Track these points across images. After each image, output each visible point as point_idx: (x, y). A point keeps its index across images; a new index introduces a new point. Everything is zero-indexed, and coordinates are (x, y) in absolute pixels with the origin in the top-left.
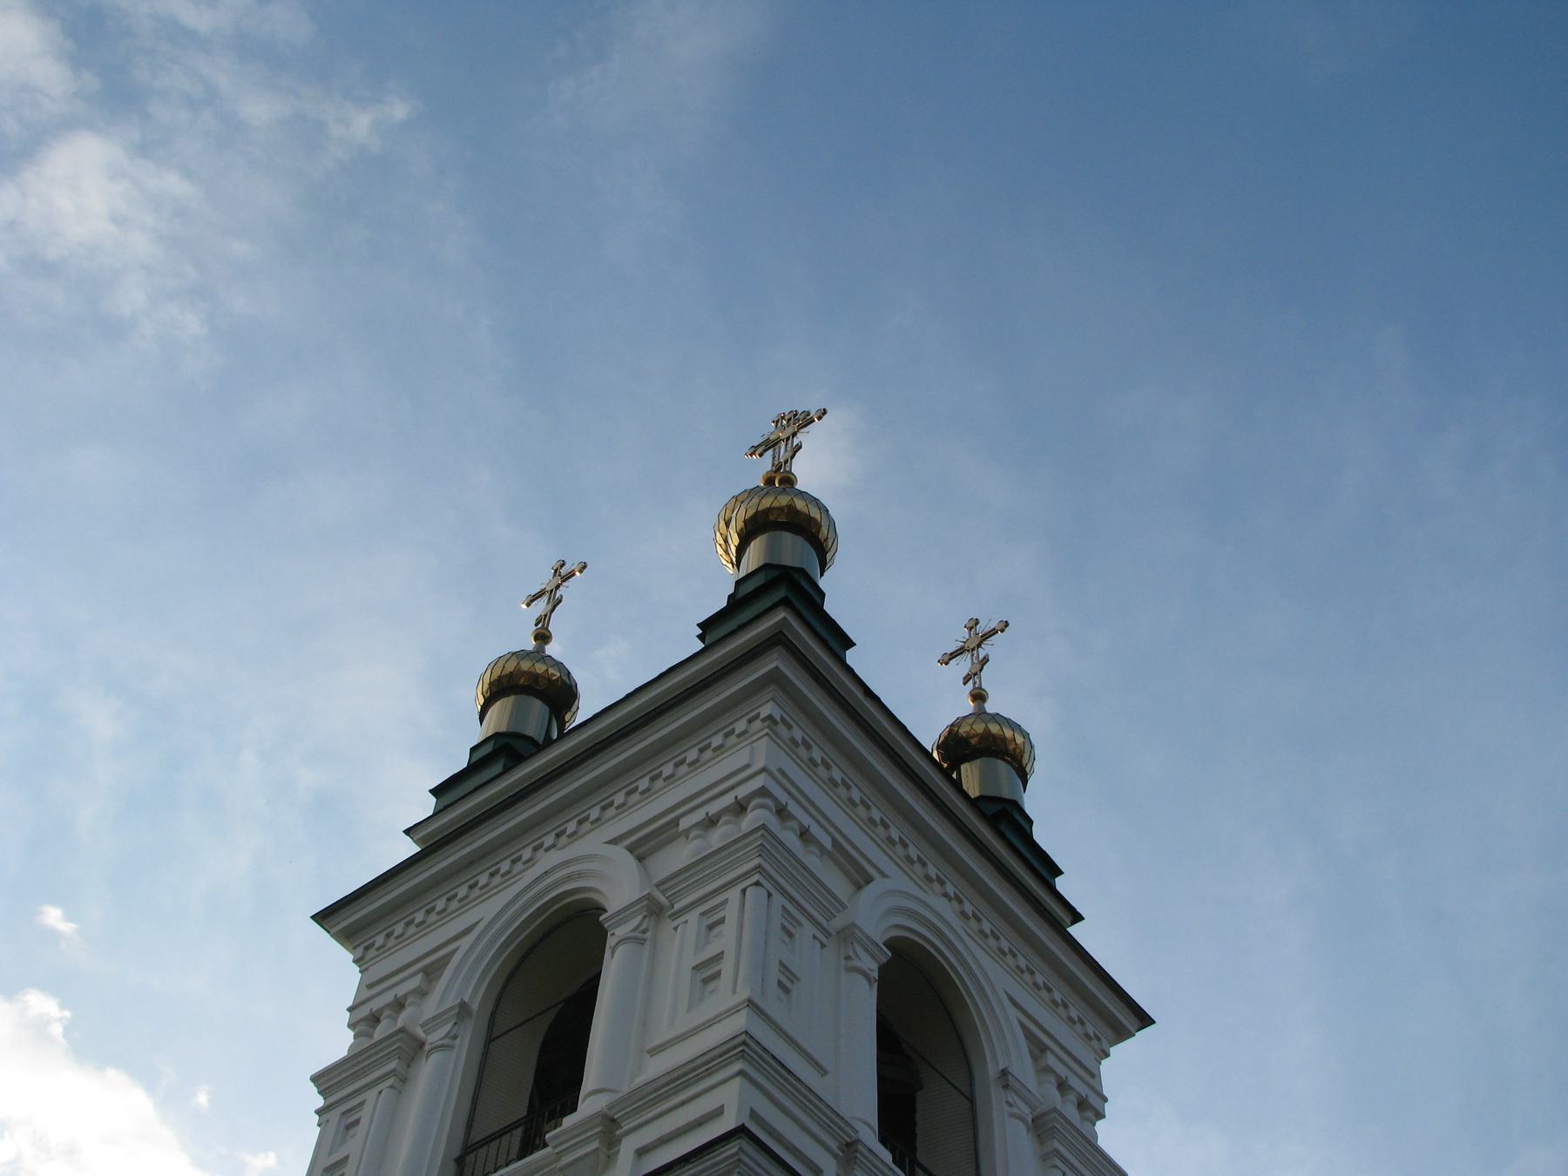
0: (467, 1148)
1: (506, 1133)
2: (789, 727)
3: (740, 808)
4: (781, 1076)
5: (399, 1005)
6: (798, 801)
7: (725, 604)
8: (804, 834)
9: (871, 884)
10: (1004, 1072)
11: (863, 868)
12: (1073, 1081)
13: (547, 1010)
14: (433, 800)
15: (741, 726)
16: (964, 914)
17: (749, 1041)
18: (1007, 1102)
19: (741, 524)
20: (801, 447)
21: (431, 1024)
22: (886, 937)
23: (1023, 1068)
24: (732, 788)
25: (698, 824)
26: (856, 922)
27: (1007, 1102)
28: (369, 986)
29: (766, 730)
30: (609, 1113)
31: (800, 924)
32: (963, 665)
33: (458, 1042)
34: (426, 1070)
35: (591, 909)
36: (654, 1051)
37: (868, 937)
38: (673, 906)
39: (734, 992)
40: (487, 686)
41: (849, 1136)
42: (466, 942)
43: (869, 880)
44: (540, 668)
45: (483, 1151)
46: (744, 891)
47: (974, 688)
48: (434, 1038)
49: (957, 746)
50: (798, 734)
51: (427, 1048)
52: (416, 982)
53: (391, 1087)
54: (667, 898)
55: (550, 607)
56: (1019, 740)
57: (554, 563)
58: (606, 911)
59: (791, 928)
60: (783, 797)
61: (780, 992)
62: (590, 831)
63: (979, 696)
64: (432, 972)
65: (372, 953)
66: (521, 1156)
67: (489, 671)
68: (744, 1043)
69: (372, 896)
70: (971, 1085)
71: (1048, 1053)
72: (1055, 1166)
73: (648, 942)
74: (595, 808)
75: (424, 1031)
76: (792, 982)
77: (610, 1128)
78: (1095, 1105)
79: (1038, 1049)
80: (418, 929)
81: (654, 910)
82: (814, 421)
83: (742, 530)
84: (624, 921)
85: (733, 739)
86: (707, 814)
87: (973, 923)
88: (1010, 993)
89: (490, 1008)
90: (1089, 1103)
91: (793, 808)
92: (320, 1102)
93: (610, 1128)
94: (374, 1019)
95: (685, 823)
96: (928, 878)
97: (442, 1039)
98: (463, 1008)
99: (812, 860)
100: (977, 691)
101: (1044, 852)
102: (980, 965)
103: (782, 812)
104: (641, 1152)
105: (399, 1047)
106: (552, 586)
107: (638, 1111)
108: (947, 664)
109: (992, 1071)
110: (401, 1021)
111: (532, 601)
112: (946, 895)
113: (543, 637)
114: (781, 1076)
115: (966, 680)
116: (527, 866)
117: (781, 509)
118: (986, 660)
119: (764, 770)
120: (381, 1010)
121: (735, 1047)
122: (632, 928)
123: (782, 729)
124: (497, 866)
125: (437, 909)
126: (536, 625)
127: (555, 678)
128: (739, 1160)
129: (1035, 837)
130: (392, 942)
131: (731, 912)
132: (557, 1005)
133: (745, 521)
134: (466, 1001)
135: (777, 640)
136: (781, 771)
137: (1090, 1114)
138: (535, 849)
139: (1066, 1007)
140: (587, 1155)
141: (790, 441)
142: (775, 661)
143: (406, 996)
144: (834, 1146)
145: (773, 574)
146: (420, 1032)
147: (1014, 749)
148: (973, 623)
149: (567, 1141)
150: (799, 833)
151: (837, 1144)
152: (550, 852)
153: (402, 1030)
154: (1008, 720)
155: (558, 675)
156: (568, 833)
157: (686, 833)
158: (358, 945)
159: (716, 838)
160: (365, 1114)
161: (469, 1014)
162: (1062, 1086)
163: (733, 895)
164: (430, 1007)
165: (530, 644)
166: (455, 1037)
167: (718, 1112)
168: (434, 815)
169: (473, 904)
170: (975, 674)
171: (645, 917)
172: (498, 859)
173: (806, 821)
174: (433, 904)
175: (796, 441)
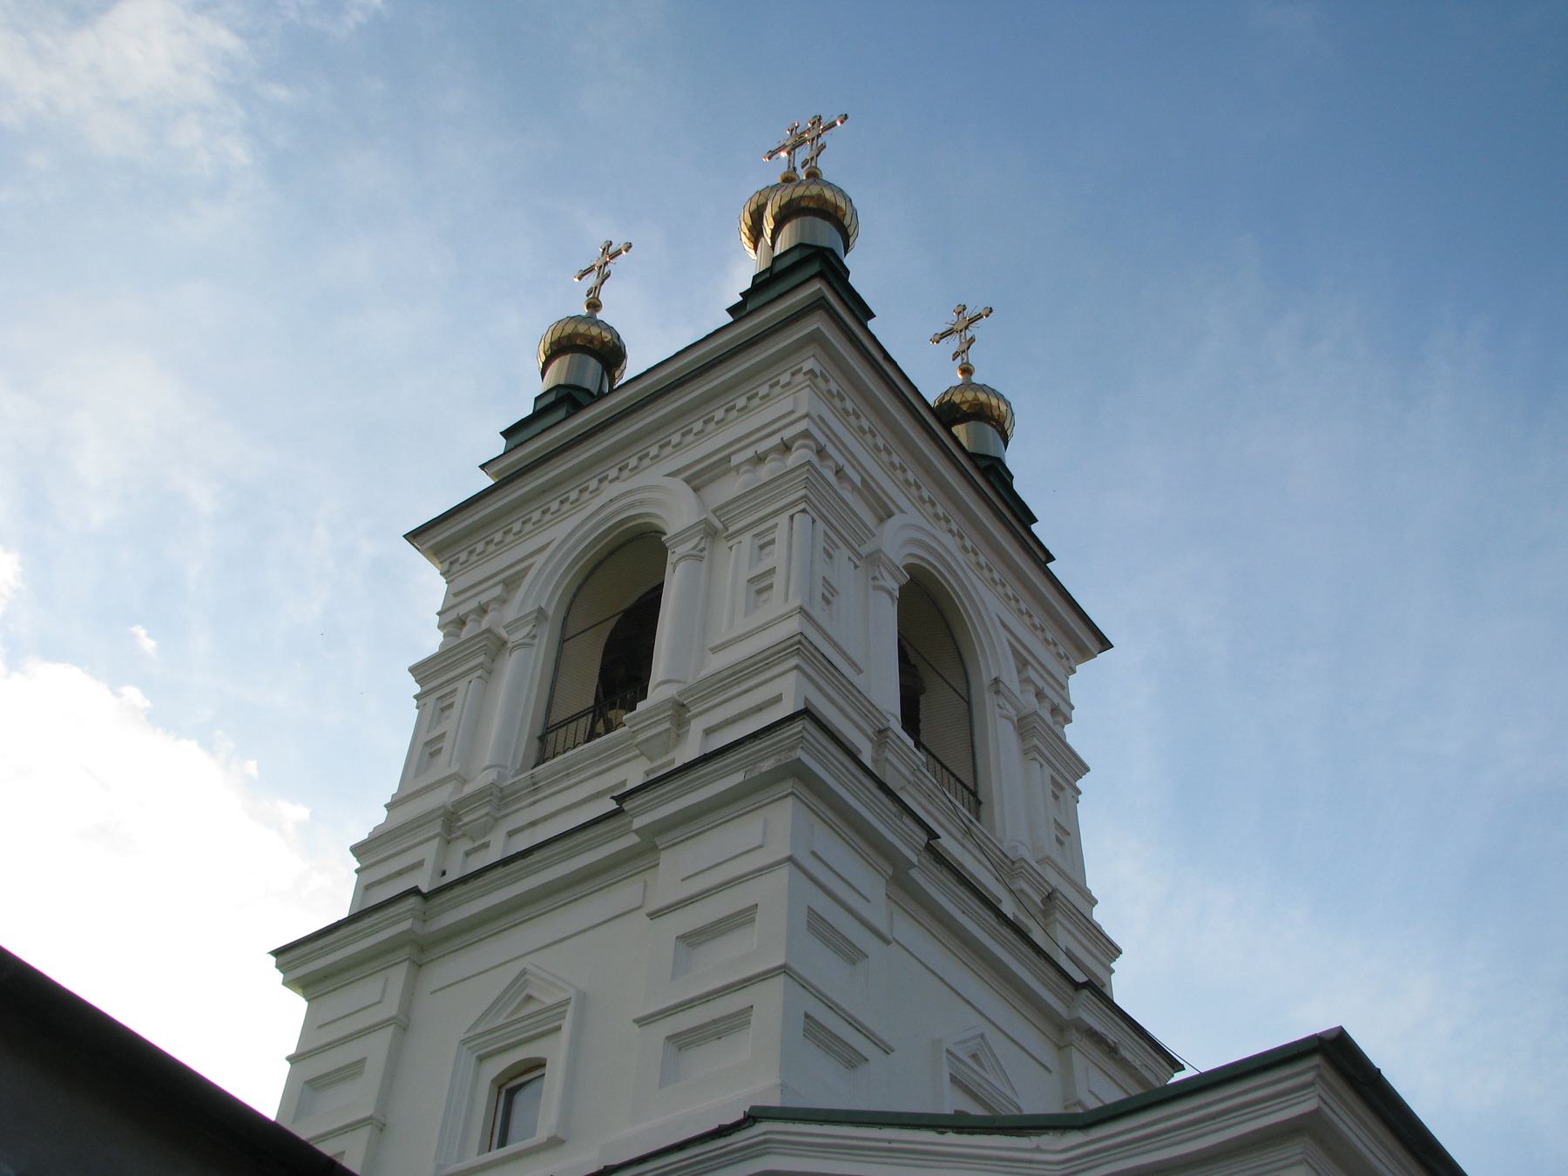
0: (548, 728)
1: (583, 716)
2: (827, 381)
3: (786, 447)
4: (829, 671)
5: (483, 610)
6: (834, 444)
7: (750, 286)
8: (839, 472)
9: (892, 518)
10: (997, 681)
11: (885, 503)
12: (1048, 692)
13: (611, 617)
14: (504, 441)
15: (785, 378)
16: (964, 548)
17: (804, 641)
18: (999, 706)
19: (776, 209)
20: (825, 147)
21: (513, 626)
22: (904, 563)
23: (1011, 680)
24: (779, 430)
25: (748, 461)
26: (883, 548)
27: (999, 706)
28: (454, 595)
29: (808, 383)
30: (678, 698)
31: (838, 547)
32: (953, 343)
33: (536, 641)
34: (510, 665)
35: (650, 532)
36: (715, 650)
37: (890, 561)
38: (727, 529)
39: (786, 600)
40: (548, 345)
41: (882, 724)
42: (540, 559)
43: (890, 515)
44: (595, 331)
45: (562, 732)
46: (792, 517)
47: (962, 364)
48: (516, 637)
49: (949, 413)
50: (834, 387)
51: (510, 645)
52: (498, 591)
53: (480, 677)
54: (722, 522)
55: (600, 281)
56: (1003, 407)
57: (602, 243)
58: (665, 534)
59: (831, 551)
60: (822, 440)
61: (823, 603)
62: (650, 466)
63: (967, 371)
64: (511, 583)
65: (457, 567)
66: (588, 741)
67: (550, 332)
68: (800, 642)
69: (472, 510)
70: (968, 690)
71: (1029, 667)
72: (1035, 759)
73: (706, 559)
74: (698, 422)
75: (507, 632)
76: (833, 595)
77: (680, 711)
78: (1065, 711)
79: (1022, 664)
80: (573, 506)
81: (710, 533)
82: (836, 124)
83: (776, 214)
84: (684, 541)
85: (777, 390)
86: (756, 452)
87: (972, 556)
88: (1003, 619)
89: (562, 615)
90: (1060, 710)
91: (830, 449)
92: (417, 689)
93: (680, 711)
94: (461, 622)
95: (735, 460)
96: (936, 516)
97: (523, 638)
98: (541, 611)
99: (848, 495)
100: (966, 366)
101: (1024, 502)
102: (975, 589)
103: (821, 452)
104: (708, 732)
105: (485, 645)
106: (601, 262)
107: (702, 699)
108: (938, 342)
109: (986, 680)
110: (485, 624)
111: (583, 275)
112: (950, 531)
113: (594, 305)
114: (829, 671)
115: (955, 356)
116: (592, 495)
117: (811, 198)
118: (972, 340)
119: (807, 415)
120: (467, 615)
121: (792, 646)
122: (689, 548)
123: (820, 381)
124: (567, 495)
125: (514, 531)
126: (587, 296)
127: (606, 340)
128: (802, 737)
129: (1016, 487)
130: (474, 558)
131: (781, 534)
132: (618, 613)
133: (780, 207)
134: (543, 606)
135: (819, 304)
136: (820, 417)
137: (1060, 719)
138: (601, 481)
139: (1043, 630)
140: (660, 734)
141: (815, 142)
142: (816, 323)
143: (488, 603)
144: (870, 731)
145: (808, 252)
146: (503, 633)
147: (999, 416)
148: (960, 309)
149: (641, 722)
150: (834, 471)
151: (873, 730)
152: (613, 484)
153: (488, 630)
154: (993, 390)
155: (610, 337)
156: (630, 467)
157: (737, 468)
158: (445, 560)
159: (765, 472)
160: (458, 699)
161: (546, 618)
162: (1039, 695)
163: (783, 519)
164: (511, 612)
165: (584, 311)
166: (534, 637)
167: (777, 699)
168: (504, 453)
169: (547, 526)
170: (963, 352)
171: (702, 538)
172: (568, 489)
173: (842, 461)
174: (457, 556)
175: (820, 141)
